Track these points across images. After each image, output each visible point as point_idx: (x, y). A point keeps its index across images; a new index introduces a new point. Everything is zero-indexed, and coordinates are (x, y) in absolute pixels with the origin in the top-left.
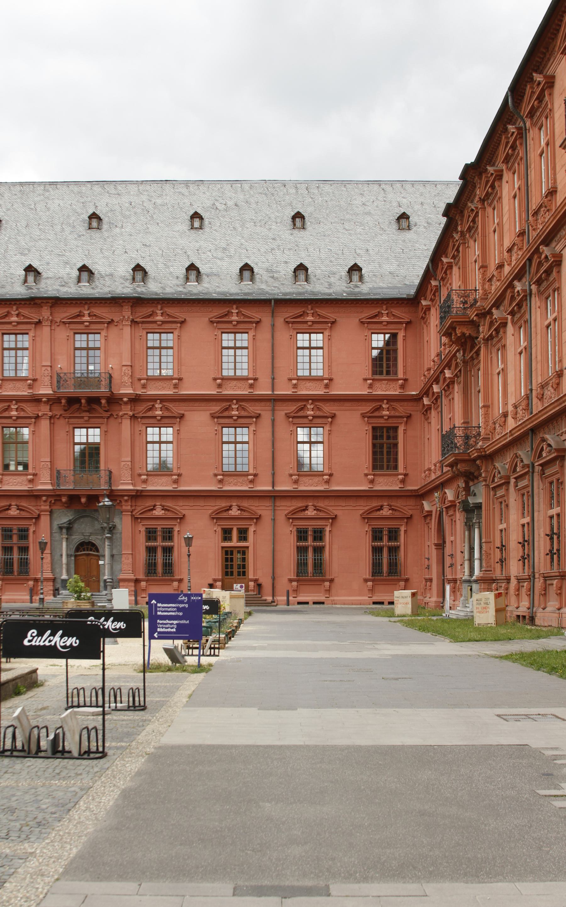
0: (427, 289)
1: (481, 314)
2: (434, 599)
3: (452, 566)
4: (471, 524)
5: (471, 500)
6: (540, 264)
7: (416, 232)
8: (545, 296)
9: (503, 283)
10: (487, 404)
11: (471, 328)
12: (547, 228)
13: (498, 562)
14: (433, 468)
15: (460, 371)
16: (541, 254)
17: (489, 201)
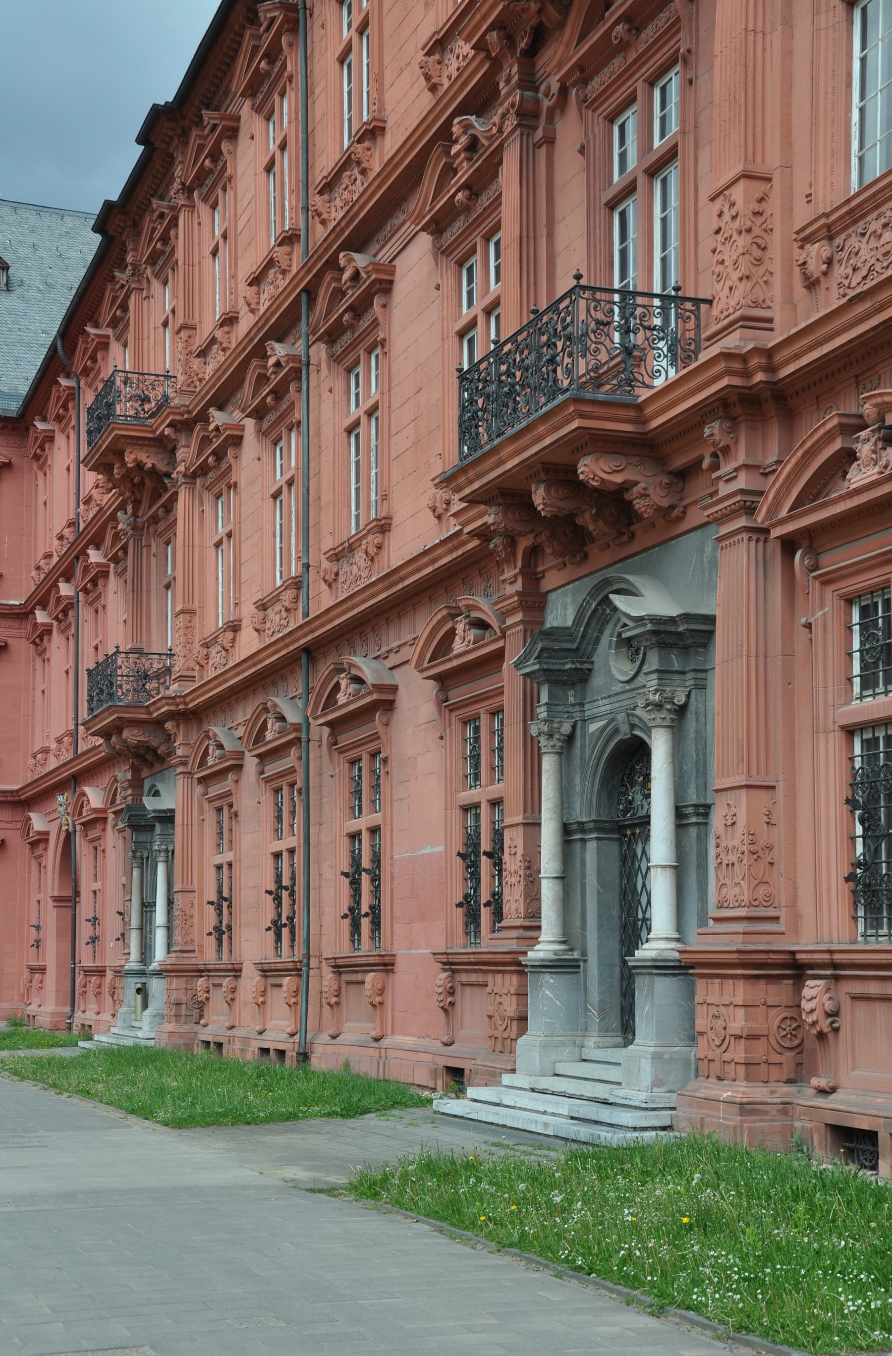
0: (49, 397)
1: (182, 422)
2: (50, 1007)
3: (93, 942)
4: (145, 855)
5: (150, 803)
6: (338, 294)
7: (21, 298)
8: (272, 438)
9: (198, 398)
10: (189, 606)
11: (157, 453)
12: (362, 207)
13: (210, 934)
14: (54, 746)
15: (125, 548)
16: (342, 270)
17: (205, 190)
